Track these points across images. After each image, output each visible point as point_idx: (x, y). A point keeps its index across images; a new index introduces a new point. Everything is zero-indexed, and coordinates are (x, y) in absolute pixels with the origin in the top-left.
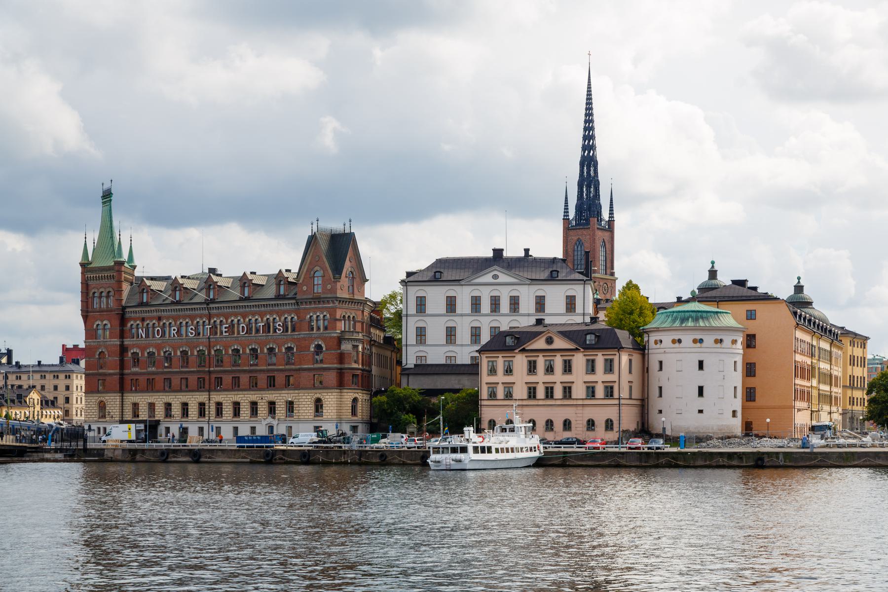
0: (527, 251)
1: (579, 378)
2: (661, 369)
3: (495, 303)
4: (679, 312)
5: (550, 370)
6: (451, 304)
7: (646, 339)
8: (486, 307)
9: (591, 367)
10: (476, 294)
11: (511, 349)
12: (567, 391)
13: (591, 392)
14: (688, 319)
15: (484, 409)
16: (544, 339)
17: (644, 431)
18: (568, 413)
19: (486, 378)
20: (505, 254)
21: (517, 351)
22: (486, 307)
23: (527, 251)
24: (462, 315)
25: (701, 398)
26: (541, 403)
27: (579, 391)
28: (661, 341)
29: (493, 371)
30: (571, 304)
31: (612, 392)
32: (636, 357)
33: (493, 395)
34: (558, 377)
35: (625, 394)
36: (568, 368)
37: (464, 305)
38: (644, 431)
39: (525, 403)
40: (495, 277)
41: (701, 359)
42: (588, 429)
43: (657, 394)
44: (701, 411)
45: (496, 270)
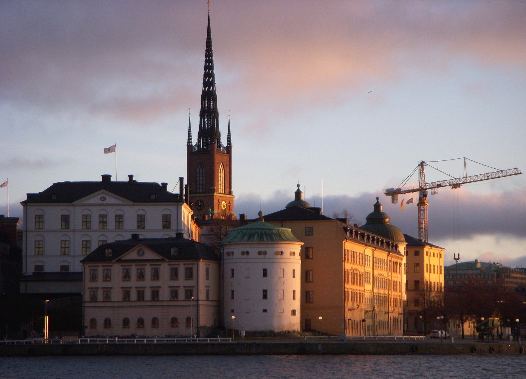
0: (131, 177)
1: (165, 283)
2: (233, 276)
3: (103, 220)
4: (247, 229)
5: (141, 276)
6: (66, 220)
7: (222, 251)
8: (95, 223)
9: (174, 274)
10: (86, 212)
11: (109, 260)
12: (155, 294)
13: (174, 294)
14: (254, 235)
15: (86, 310)
16: (136, 251)
17: (220, 326)
18: (156, 313)
19: (88, 284)
20: (113, 179)
21: (114, 261)
22: (95, 223)
23: (131, 177)
24: (74, 231)
25: (265, 300)
26: (133, 304)
27: (165, 295)
28: (233, 253)
29: (94, 278)
30: (119, 222)
31: (129, 296)
32: (212, 266)
33: (94, 299)
34: (148, 283)
35: (202, 296)
36: (156, 276)
37: (76, 222)
38: (220, 326)
39: (120, 304)
40: (103, 199)
41: (265, 268)
42: (172, 326)
43: (230, 296)
44: (265, 311)
45: (102, 193)
